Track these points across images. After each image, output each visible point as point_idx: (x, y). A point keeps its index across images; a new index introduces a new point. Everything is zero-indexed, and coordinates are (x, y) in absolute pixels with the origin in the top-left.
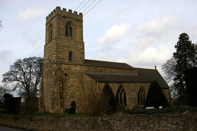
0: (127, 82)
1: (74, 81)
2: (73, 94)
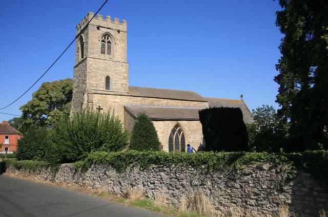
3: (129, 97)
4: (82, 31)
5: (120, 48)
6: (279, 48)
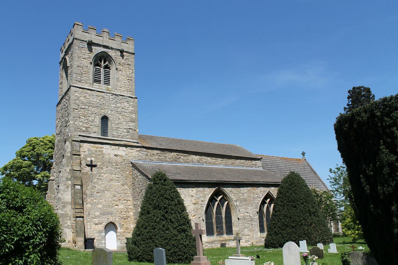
1: (111, 180)
2: (109, 206)
3: (139, 149)
4: (66, 53)
5: (122, 76)
6: (349, 92)
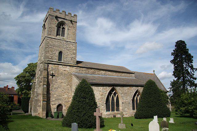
0: (70, 66)
2: (60, 96)
